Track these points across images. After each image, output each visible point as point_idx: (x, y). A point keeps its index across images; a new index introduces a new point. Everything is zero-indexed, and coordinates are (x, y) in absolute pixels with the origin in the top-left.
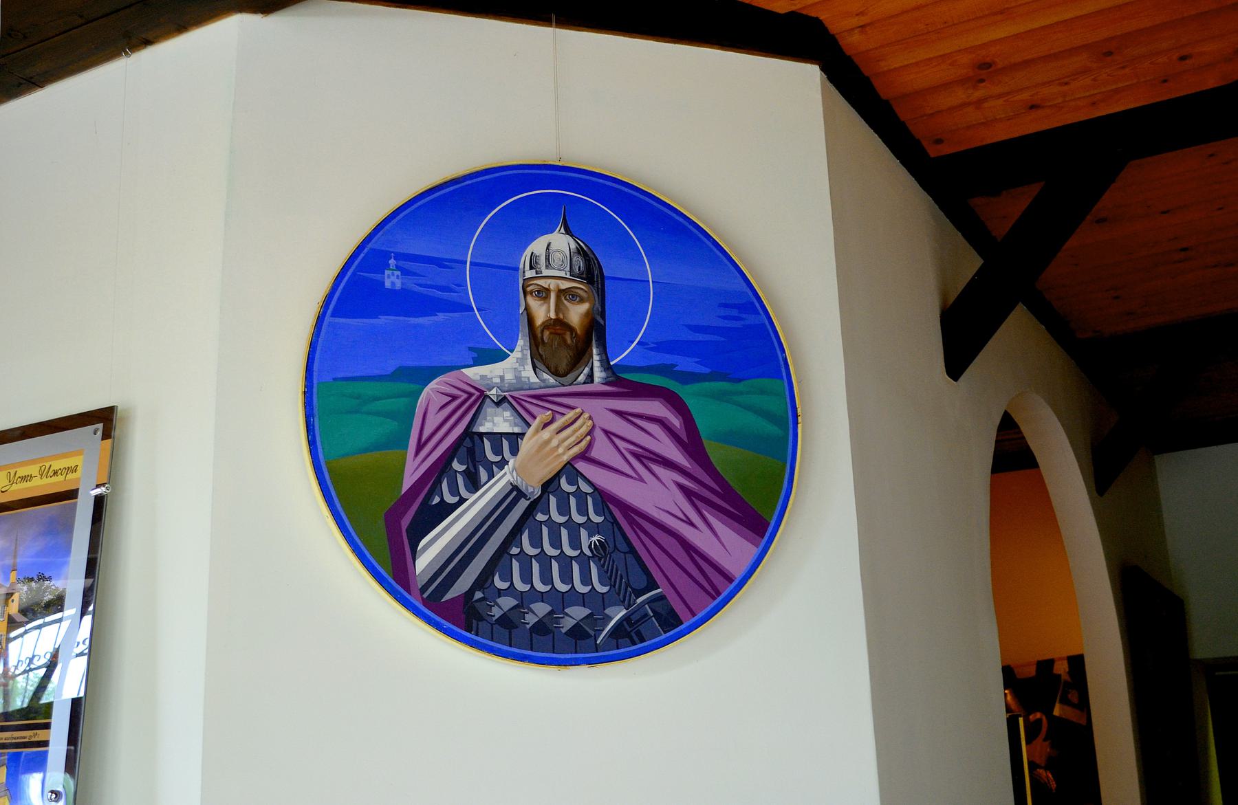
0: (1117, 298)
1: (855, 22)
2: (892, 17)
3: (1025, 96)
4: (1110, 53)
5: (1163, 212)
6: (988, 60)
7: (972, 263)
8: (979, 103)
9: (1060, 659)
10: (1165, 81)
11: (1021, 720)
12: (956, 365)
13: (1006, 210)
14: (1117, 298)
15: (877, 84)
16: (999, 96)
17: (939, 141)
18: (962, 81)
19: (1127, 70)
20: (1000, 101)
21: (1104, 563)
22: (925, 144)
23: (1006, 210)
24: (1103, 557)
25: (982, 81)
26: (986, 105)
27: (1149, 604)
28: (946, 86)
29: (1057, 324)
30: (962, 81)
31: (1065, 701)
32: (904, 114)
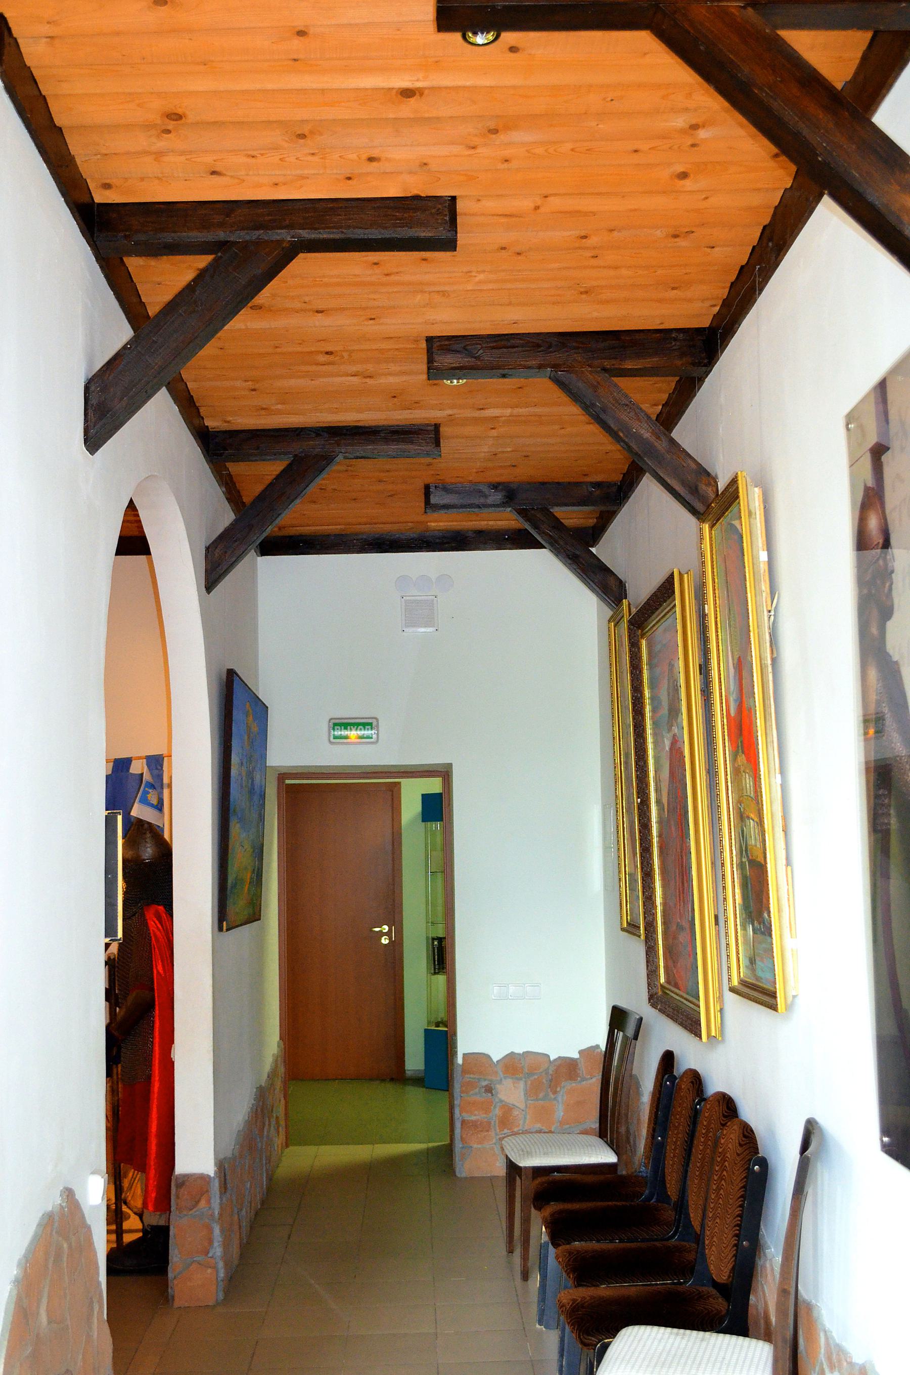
0: (254, 390)
1: (46, 29)
2: (569, 194)
3: (209, 159)
4: (302, 136)
5: (318, 312)
6: (180, 111)
7: (121, 333)
8: (159, 155)
9: (139, 758)
10: (349, 178)
11: (120, 818)
12: (94, 440)
13: (165, 279)
14: (254, 390)
15: (55, 108)
16: (182, 153)
17: (107, 186)
18: (148, 127)
19: (315, 159)
20: (183, 158)
21: (204, 664)
22: (92, 186)
23: (165, 279)
24: (598, 715)
25: (169, 132)
26: (166, 159)
27: (236, 705)
28: (128, 127)
29: (188, 406)
30: (148, 127)
31: (145, 801)
32: (76, 147)
